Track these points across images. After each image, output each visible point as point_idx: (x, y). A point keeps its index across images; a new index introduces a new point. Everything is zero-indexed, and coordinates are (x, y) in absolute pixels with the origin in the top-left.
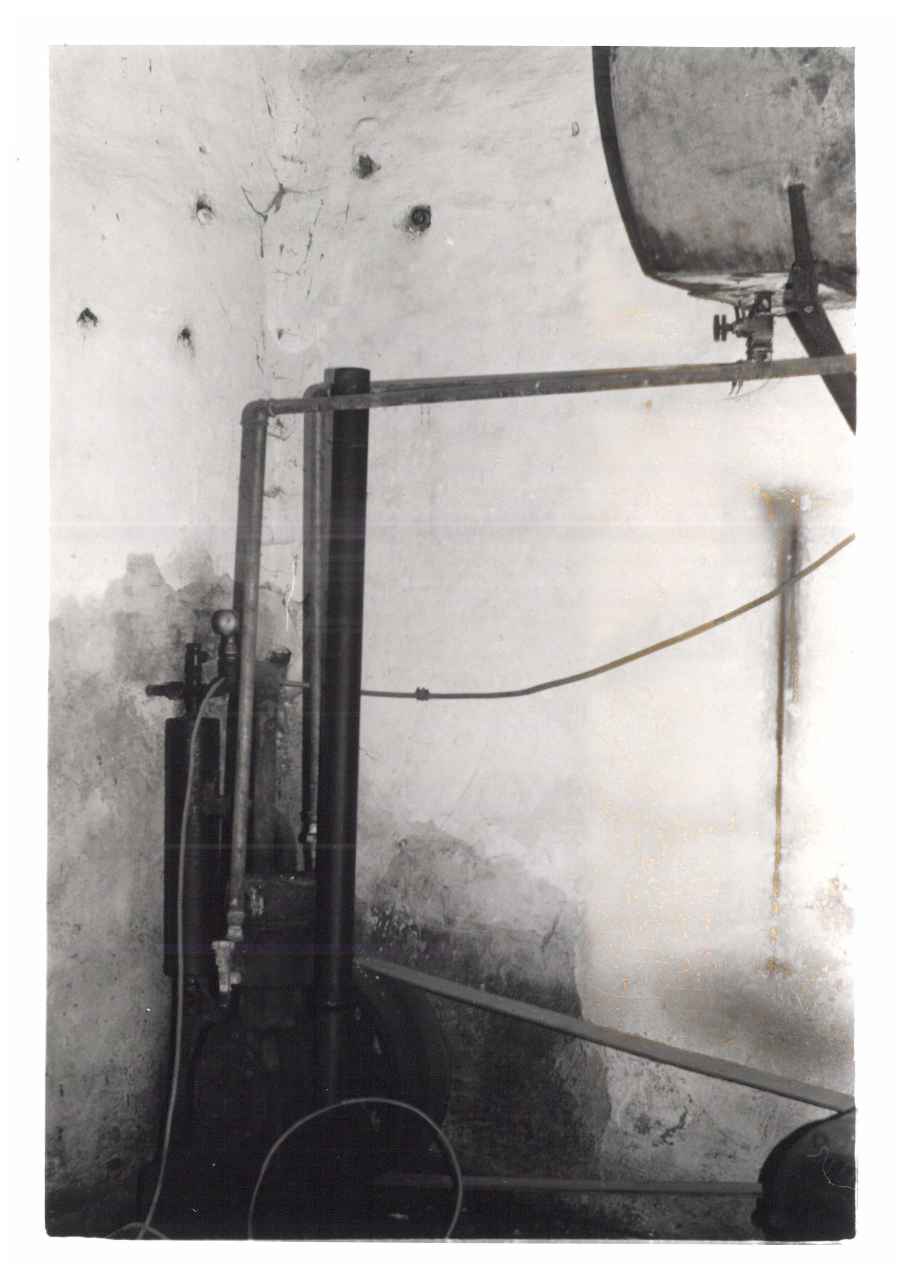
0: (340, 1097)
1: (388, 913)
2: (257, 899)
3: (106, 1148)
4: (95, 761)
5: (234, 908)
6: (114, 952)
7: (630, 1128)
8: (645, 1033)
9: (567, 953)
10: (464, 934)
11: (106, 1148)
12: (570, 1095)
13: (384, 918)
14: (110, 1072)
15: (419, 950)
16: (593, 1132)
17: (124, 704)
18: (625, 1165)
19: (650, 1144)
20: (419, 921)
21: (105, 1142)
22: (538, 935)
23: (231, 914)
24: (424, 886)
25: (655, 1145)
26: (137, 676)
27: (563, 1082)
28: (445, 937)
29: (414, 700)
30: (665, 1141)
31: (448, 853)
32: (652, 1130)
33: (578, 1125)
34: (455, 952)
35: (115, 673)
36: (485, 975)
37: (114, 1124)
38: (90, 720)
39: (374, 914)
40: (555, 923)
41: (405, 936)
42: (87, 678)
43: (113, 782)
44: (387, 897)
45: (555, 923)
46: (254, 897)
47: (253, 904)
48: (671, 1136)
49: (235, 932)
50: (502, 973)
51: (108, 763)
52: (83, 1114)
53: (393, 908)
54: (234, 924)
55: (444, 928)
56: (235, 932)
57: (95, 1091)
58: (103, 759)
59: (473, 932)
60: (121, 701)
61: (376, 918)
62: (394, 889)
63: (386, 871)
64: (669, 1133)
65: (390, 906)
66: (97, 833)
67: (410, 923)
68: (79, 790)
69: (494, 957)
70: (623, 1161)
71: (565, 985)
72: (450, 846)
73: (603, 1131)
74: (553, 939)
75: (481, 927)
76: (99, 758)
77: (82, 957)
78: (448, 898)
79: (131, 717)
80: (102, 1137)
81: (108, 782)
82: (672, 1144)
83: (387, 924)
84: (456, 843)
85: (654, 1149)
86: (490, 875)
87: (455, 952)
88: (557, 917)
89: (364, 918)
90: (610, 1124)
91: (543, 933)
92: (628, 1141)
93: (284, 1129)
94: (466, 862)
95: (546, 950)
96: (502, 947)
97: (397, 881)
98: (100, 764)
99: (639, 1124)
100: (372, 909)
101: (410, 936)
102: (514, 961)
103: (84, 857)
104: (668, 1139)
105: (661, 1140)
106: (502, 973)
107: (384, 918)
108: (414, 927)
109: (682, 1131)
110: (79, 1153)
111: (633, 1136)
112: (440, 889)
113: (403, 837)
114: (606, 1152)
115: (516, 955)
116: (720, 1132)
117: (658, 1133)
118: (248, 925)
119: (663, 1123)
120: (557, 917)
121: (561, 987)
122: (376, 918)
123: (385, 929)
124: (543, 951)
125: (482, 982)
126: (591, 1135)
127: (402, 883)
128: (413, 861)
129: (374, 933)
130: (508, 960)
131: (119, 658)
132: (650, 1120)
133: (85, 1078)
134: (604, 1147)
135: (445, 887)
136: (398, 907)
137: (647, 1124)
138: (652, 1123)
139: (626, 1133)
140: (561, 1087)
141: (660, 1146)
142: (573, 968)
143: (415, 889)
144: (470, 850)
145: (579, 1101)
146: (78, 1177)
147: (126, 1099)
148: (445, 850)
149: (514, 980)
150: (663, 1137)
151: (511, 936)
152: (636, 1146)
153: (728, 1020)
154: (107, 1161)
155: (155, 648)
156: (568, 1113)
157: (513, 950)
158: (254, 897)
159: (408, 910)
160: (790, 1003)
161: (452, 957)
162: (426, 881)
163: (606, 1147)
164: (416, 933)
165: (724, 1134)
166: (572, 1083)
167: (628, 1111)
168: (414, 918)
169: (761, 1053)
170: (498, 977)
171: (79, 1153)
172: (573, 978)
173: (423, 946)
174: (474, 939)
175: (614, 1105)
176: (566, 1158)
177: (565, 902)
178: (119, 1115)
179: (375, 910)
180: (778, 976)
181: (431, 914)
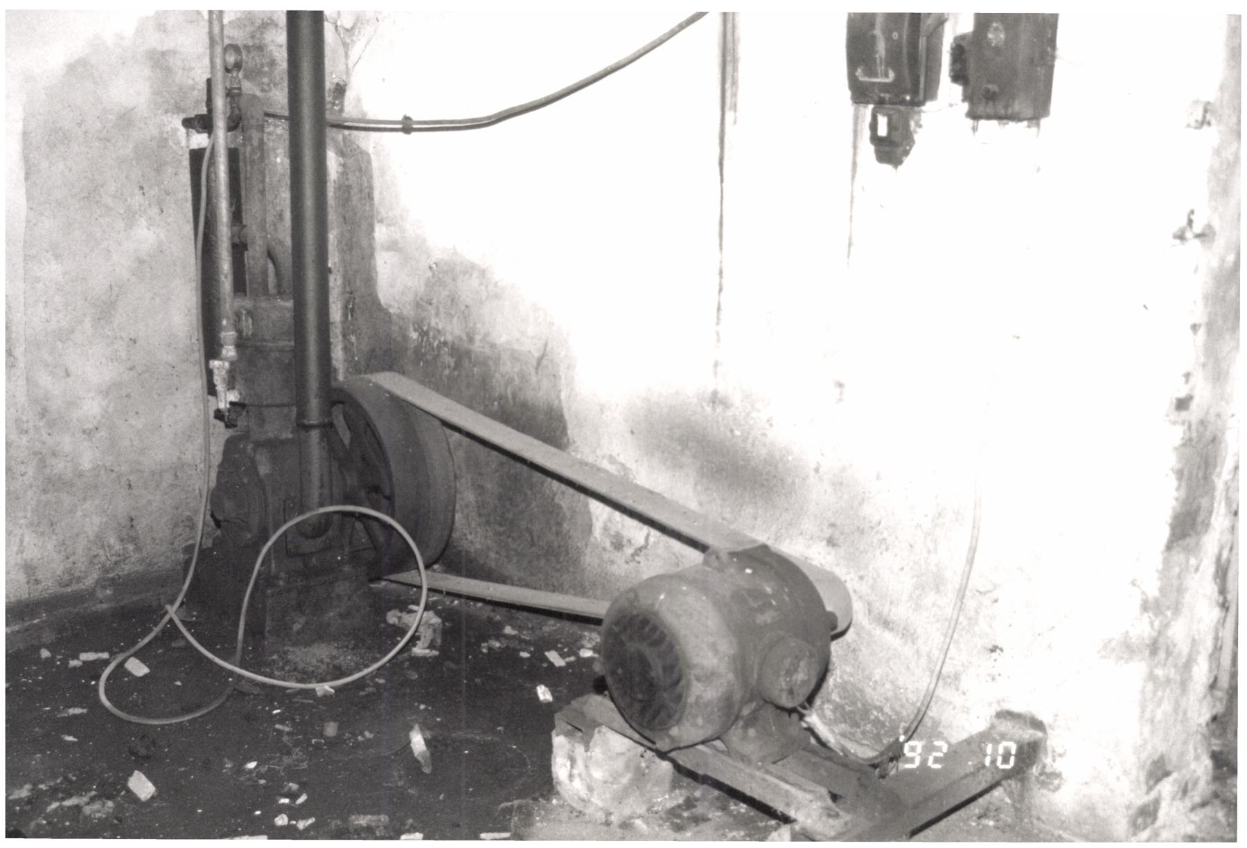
0: (321, 505)
1: (425, 328)
2: (247, 321)
3: (181, 535)
4: (137, 191)
5: (225, 329)
6: (174, 364)
7: (608, 544)
8: (618, 455)
9: (554, 376)
10: (481, 352)
11: (181, 535)
12: (560, 507)
13: (423, 334)
14: (178, 469)
15: (449, 367)
16: (579, 544)
17: (165, 136)
18: (604, 578)
19: (623, 560)
20: (449, 338)
21: (179, 530)
22: (533, 356)
23: (223, 334)
24: (452, 304)
25: (627, 562)
26: (178, 109)
27: (555, 495)
28: (468, 353)
29: (401, 134)
30: (634, 560)
31: (467, 276)
32: (625, 549)
33: (567, 537)
34: (475, 370)
35: (152, 106)
36: (497, 394)
37: (187, 513)
38: (128, 151)
39: (415, 330)
40: (546, 345)
41: (439, 351)
42: (123, 112)
43: (159, 211)
44: (423, 314)
45: (546, 345)
46: (244, 318)
47: (244, 324)
48: (638, 555)
49: (229, 351)
50: (509, 392)
51: (153, 193)
52: (154, 504)
53: (429, 324)
54: (227, 344)
55: (466, 345)
56: (229, 351)
57: (164, 484)
58: (146, 189)
59: (487, 351)
60: (161, 133)
61: (417, 334)
62: (430, 307)
63: (423, 289)
64: (639, 550)
65: (426, 322)
66: (146, 258)
67: (442, 339)
68: (123, 219)
69: (503, 376)
70: (603, 575)
71: (554, 407)
72: (469, 269)
73: (586, 545)
74: (544, 362)
75: (493, 346)
76: (142, 188)
77: (140, 369)
78: (469, 316)
79: (175, 147)
80: (176, 525)
81: (154, 211)
82: (639, 562)
83: (425, 339)
84: (473, 266)
85: (626, 566)
86: (497, 296)
87: (475, 370)
88: (547, 339)
89: (408, 334)
90: (592, 539)
91: (536, 355)
92: (606, 556)
93: (276, 529)
94: (481, 284)
95: (540, 372)
96: (508, 367)
97: (432, 299)
98: (144, 194)
99: (614, 541)
100: (414, 325)
101: (442, 352)
102: (517, 381)
103: (133, 279)
104: (637, 558)
105: (631, 558)
106: (509, 392)
107: (423, 334)
108: (445, 343)
109: (646, 551)
110: (154, 539)
111: (610, 551)
112: (463, 308)
113: (434, 260)
114: (589, 565)
115: (518, 374)
116: (674, 554)
117: (629, 551)
118: (240, 345)
119: (633, 542)
120: (547, 339)
121: (551, 408)
122: (417, 334)
123: (424, 344)
124: (537, 373)
125: (495, 400)
126: (578, 548)
127: (435, 301)
128: (443, 284)
129: (415, 347)
130: (512, 380)
131: (157, 93)
132: (623, 537)
133: (153, 473)
134: (588, 559)
135: (467, 306)
136: (433, 324)
137: (621, 542)
138: (625, 542)
139: (604, 549)
140: (553, 499)
141: (631, 564)
142: (560, 391)
143: (444, 308)
144: (483, 273)
145: (568, 515)
146: (155, 560)
147: (197, 491)
148: (465, 273)
149: (517, 400)
150: (633, 555)
151: (515, 357)
152: (612, 562)
153: (679, 448)
154: (183, 546)
155: (197, 84)
156: (559, 524)
157: (516, 370)
158: (244, 318)
159: (440, 327)
160: (729, 434)
161: (473, 375)
162: (452, 301)
163: (589, 560)
164: (447, 349)
165: (677, 558)
166: (561, 496)
167: (606, 529)
168: (445, 335)
169: (705, 480)
170: (506, 397)
171: (154, 539)
172: (560, 401)
173: (452, 362)
174: (488, 357)
175: (594, 520)
176: (558, 567)
177: (553, 324)
178: (191, 505)
179: (416, 326)
180: (719, 409)
181: (457, 332)
